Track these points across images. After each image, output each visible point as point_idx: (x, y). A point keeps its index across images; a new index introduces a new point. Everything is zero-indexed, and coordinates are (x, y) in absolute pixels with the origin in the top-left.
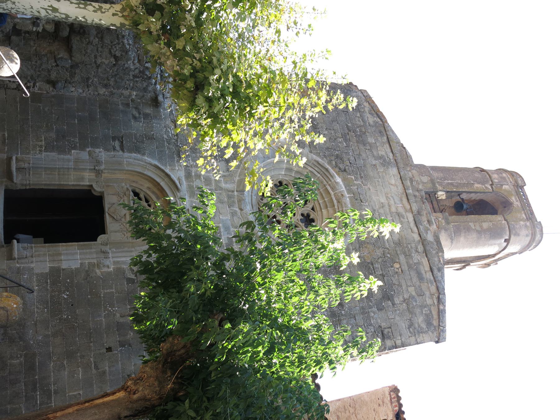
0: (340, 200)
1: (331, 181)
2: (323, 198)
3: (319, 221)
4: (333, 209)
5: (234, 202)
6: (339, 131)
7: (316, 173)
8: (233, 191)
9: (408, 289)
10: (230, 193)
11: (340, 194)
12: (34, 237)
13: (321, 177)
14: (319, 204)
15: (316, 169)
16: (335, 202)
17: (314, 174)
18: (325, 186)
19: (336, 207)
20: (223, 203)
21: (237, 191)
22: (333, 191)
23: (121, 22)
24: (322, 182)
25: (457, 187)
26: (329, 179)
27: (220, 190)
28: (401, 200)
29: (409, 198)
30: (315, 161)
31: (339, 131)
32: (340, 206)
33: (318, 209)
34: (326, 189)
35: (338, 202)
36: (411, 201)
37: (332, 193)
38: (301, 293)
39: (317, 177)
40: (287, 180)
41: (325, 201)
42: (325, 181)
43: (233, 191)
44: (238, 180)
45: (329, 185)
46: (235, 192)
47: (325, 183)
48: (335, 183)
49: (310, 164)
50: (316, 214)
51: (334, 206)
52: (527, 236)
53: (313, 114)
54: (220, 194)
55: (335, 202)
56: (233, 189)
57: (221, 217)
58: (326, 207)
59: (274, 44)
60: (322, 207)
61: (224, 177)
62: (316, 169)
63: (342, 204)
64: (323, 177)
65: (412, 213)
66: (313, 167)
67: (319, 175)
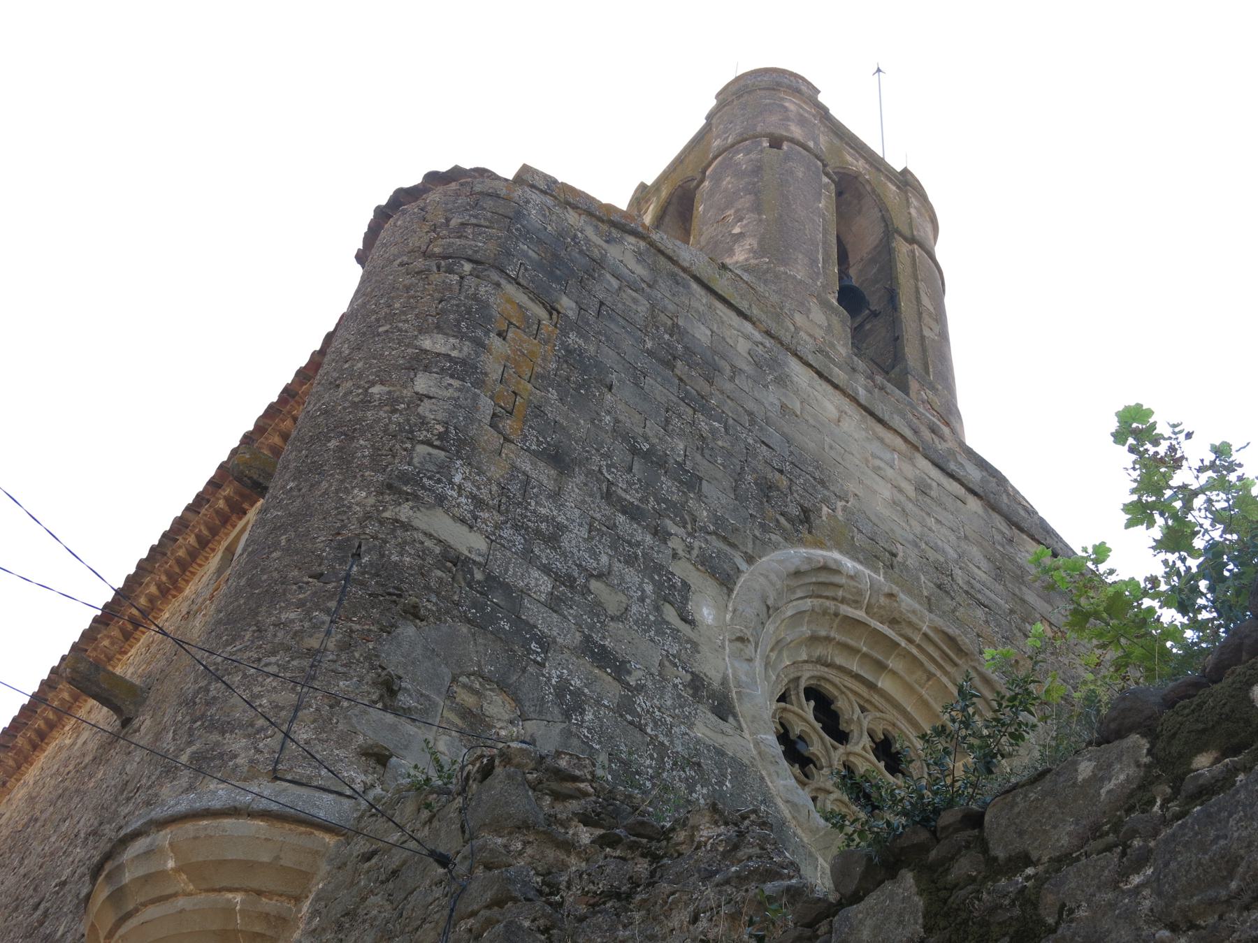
0: (896, 615)
2: (853, 651)
3: (899, 723)
4: (899, 655)
12: (819, 92)
14: (857, 677)
16: (885, 629)
18: (836, 615)
19: (903, 643)
23: (1112, 434)
32: (909, 632)
35: (893, 622)
37: (860, 614)
38: (516, 553)
41: (865, 655)
45: (843, 601)
48: (852, 583)
52: (1135, 481)
55: (885, 629)
58: (881, 667)
59: (778, 701)
60: (870, 678)
63: (910, 624)
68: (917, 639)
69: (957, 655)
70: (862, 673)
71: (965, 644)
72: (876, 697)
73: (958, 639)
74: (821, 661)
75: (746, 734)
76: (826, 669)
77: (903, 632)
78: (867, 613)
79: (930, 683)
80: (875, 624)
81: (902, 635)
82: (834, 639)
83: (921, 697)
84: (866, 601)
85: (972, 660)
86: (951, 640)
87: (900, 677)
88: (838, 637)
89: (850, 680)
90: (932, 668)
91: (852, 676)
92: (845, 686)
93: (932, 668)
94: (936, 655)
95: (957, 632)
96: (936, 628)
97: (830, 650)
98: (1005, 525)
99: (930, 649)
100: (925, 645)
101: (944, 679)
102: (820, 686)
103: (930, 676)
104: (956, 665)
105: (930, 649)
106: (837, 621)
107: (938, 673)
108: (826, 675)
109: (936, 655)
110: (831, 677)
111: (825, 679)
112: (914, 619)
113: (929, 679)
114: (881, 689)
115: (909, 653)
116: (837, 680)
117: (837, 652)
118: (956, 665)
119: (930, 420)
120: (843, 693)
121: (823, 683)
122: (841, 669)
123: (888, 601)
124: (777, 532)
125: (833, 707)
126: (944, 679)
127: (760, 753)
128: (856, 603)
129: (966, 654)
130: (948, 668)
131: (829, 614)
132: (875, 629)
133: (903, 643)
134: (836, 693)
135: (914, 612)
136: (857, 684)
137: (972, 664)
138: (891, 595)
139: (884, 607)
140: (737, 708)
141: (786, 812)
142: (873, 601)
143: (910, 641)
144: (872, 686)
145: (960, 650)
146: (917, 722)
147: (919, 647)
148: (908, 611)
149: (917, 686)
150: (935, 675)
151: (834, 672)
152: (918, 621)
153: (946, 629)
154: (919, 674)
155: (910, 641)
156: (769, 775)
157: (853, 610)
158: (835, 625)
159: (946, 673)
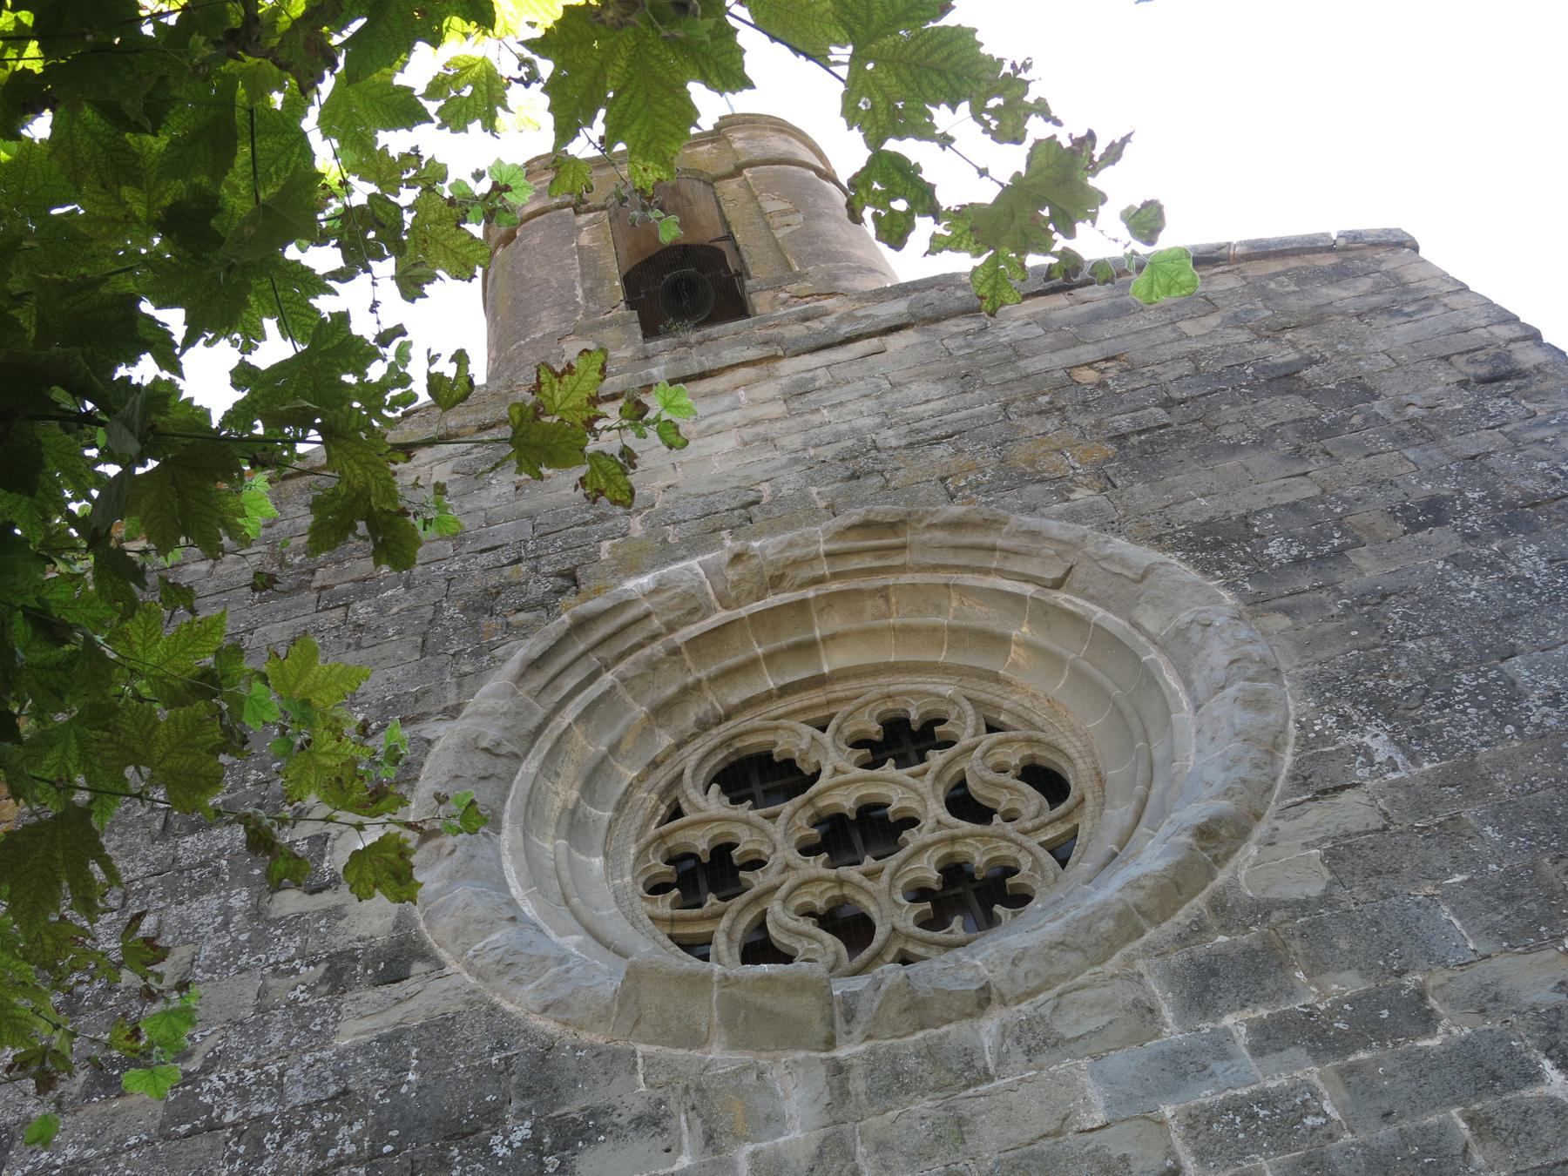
0: (769, 572)
1: (647, 615)
3: (893, 689)
4: (820, 611)
5: (930, 1053)
6: (307, 619)
7: (594, 691)
8: (839, 1070)
9: (639, 1122)
10: (858, 1085)
11: (732, 575)
13: (621, 667)
14: (785, 691)
15: (569, 683)
17: (601, 698)
18: (675, 651)
19: (810, 593)
20: (960, 1122)
21: (830, 1043)
22: (710, 611)
24: (653, 665)
25: (600, 281)
26: (637, 621)
27: (848, 1155)
28: (713, 394)
29: (697, 370)
30: (521, 678)
31: (307, 619)
32: (807, 573)
33: (815, 697)
34: (692, 642)
35: (776, 582)
36: (709, 365)
37: (719, 617)
39: (621, 690)
40: (642, 854)
42: (647, 651)
43: (839, 1070)
44: (733, 1046)
45: (671, 628)
46: (842, 1053)
47: (657, 648)
49: (541, 711)
50: (848, 708)
51: (803, 603)
53: (237, 567)
54: (881, 1146)
55: (773, 600)
56: (821, 1073)
57: (1099, 1117)
58: (807, 648)
60: (805, 674)
61: (724, 1141)
62: (569, 683)
63: (796, 563)
64: (621, 657)
65: (780, 358)
66: (557, 697)
67: (608, 678)
68: (824, 569)
69: (896, 535)
70: (788, 679)
71: (886, 513)
72: (837, 687)
73: (872, 516)
74: (704, 726)
75: (453, 967)
76: (730, 724)
77: (798, 582)
78: (727, 608)
79: (893, 600)
80: (743, 612)
81: (801, 586)
82: (699, 681)
83: (894, 629)
84: (713, 597)
85: (920, 521)
86: (867, 526)
87: (845, 635)
88: (702, 674)
89: (781, 703)
90: (878, 582)
91: (780, 697)
92: (777, 718)
93: (878, 582)
94: (868, 562)
95: (862, 511)
96: (836, 533)
97: (711, 697)
98: (968, 320)
99: (855, 563)
100: (841, 566)
101: (905, 579)
102: (738, 750)
103: (883, 592)
104: (903, 547)
105: (855, 563)
106: (686, 656)
107: (891, 580)
108: (733, 731)
109: (868, 562)
110: (749, 725)
111: (734, 737)
112: (796, 553)
113: (887, 599)
114: (832, 672)
115: (830, 596)
116: (757, 722)
117: (725, 690)
118: (903, 547)
119: (795, 312)
120: (776, 729)
121: (738, 744)
122: (748, 704)
123: (740, 568)
124: (510, 638)
125: (776, 759)
126: (905, 579)
127: (479, 976)
128: (696, 611)
129: (903, 522)
130: (897, 560)
131: (661, 661)
132: (752, 616)
133: (810, 593)
134: (770, 737)
135: (791, 545)
136: (797, 697)
137: (924, 524)
138: (737, 558)
139: (742, 580)
140: (430, 939)
141: (548, 1025)
142: (720, 587)
143: (819, 581)
144: (819, 681)
145: (893, 527)
146: (916, 663)
147: (835, 576)
148: (781, 552)
149: (883, 622)
150: (886, 587)
151: (748, 715)
152: (805, 550)
153: (848, 522)
154: (870, 606)
155: (819, 581)
156: (504, 994)
157: (703, 623)
158: (689, 663)
159: (902, 569)
